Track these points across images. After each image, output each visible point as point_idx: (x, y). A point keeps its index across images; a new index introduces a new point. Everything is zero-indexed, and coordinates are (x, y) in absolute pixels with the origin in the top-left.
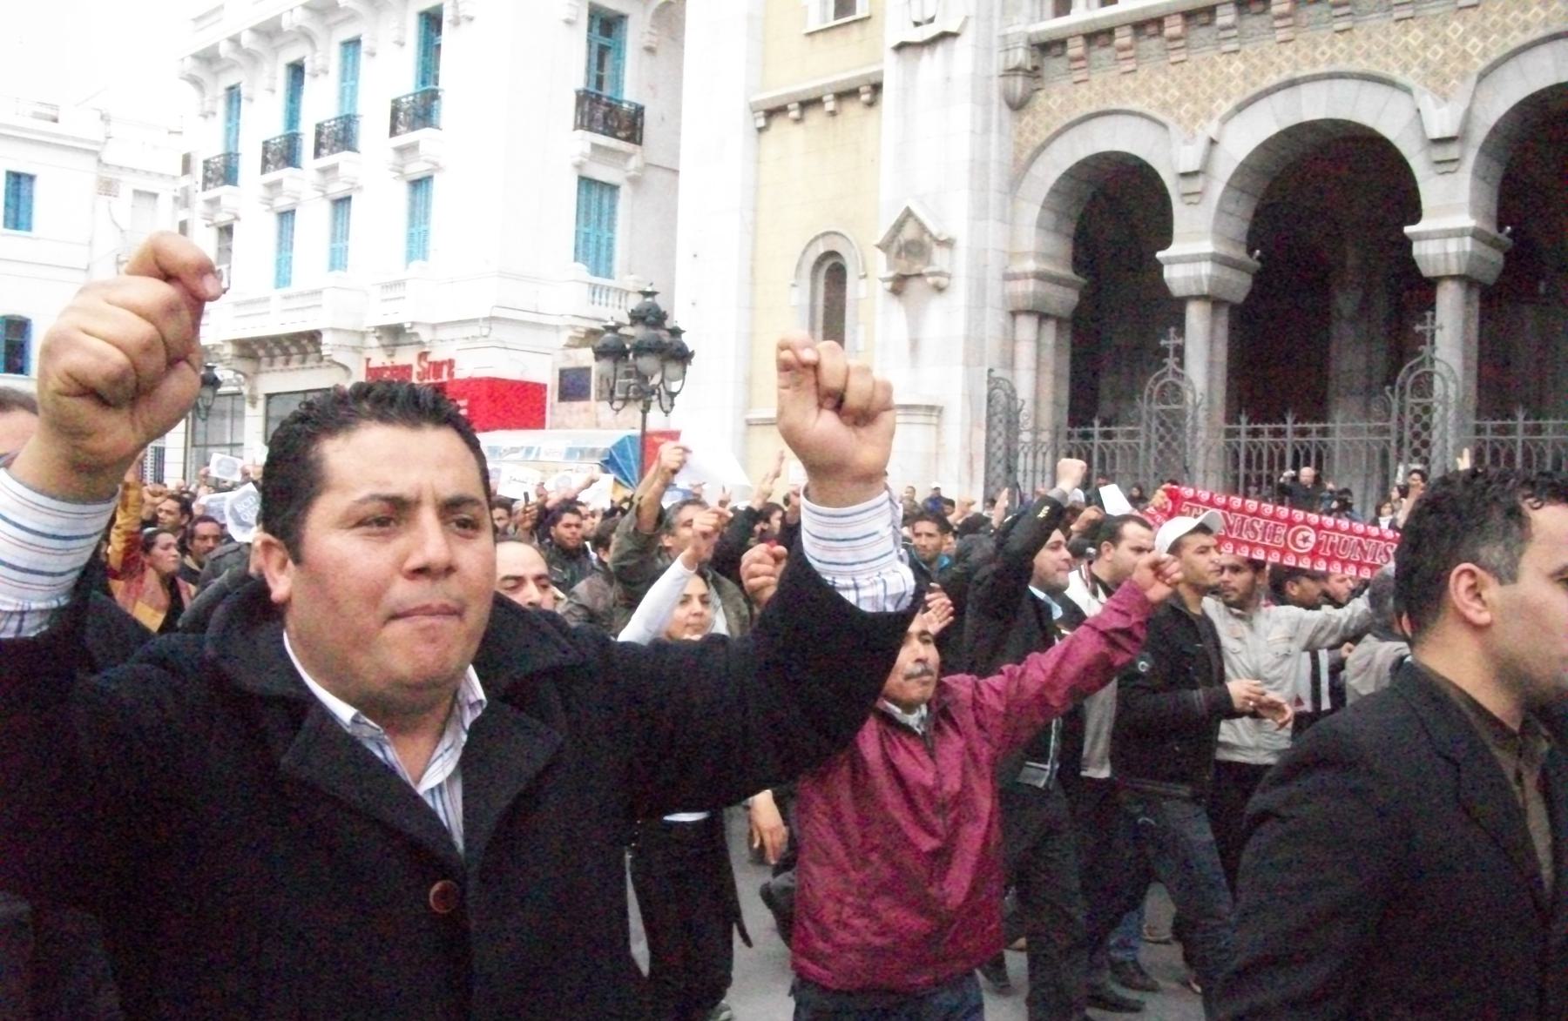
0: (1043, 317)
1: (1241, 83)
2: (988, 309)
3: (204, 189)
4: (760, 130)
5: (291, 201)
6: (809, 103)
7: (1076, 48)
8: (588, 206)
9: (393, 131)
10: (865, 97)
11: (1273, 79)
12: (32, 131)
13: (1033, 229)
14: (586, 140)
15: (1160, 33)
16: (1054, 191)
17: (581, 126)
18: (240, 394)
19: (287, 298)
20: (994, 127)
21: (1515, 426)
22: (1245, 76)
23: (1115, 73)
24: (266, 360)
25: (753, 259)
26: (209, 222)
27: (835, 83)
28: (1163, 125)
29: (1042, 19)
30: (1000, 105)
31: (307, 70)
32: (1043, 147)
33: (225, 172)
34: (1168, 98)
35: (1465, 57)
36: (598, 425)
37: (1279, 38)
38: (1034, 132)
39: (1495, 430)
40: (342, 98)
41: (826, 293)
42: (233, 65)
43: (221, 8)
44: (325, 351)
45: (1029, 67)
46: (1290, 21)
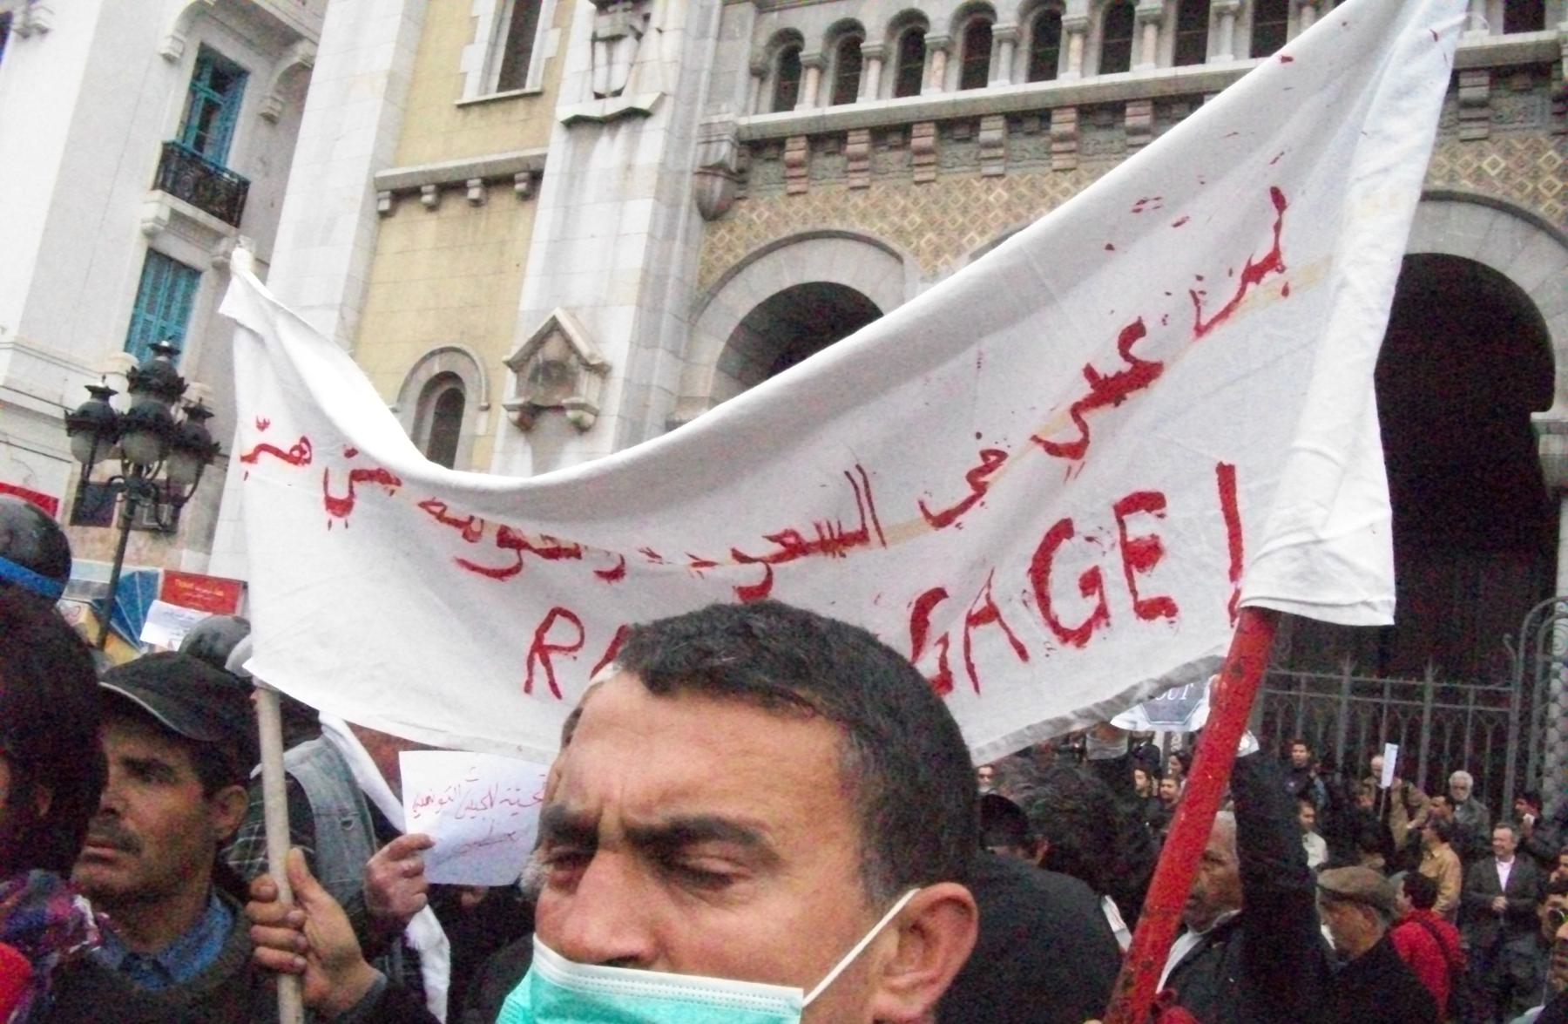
1: (1000, 213)
4: (384, 215)
6: (450, 187)
7: (796, 151)
10: (520, 187)
13: (713, 369)
15: (905, 145)
16: (745, 324)
20: (680, 233)
21: (1423, 687)
22: (1008, 207)
23: (843, 187)
27: (487, 165)
28: (899, 258)
29: (756, 112)
30: (690, 211)
32: (738, 269)
34: (905, 223)
37: (1056, 164)
39: (1395, 691)
41: (434, 429)
45: (733, 168)
46: (1073, 145)
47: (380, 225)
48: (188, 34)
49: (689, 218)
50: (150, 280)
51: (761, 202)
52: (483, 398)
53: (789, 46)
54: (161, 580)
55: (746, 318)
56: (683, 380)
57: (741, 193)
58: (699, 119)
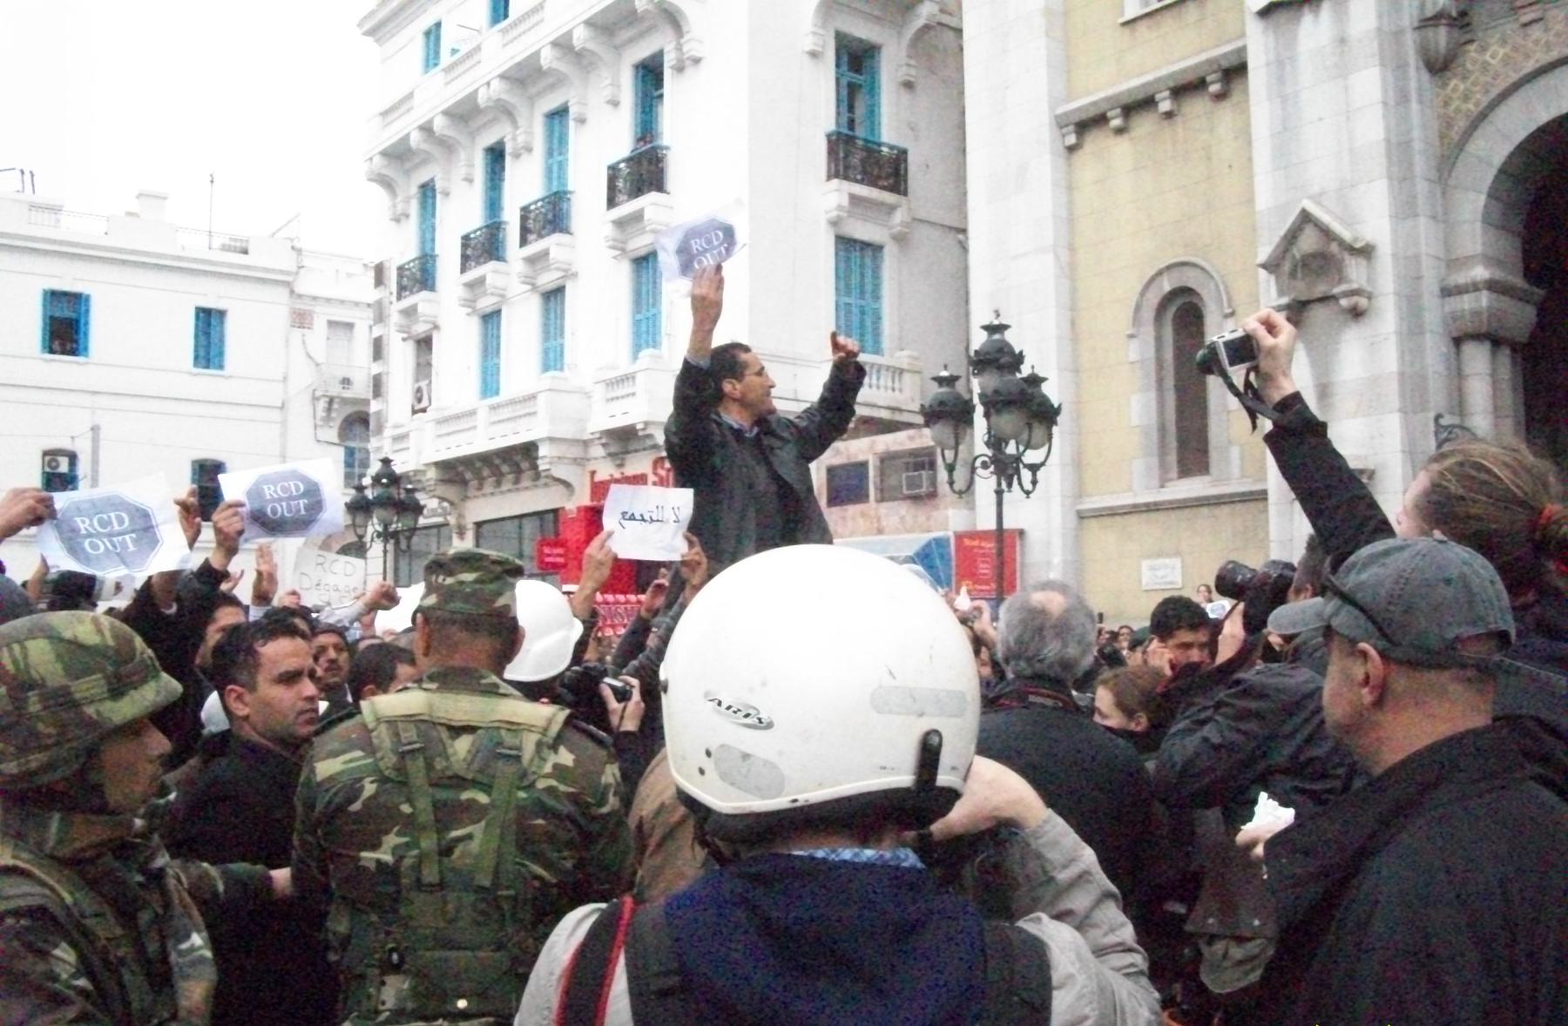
0: (1496, 342)
2: (1428, 336)
3: (399, 298)
4: (1071, 149)
5: (494, 300)
6: (1137, 106)
8: (848, 267)
9: (612, 202)
12: (222, 264)
13: (1478, 225)
14: (837, 194)
16: (1502, 171)
17: (837, 176)
18: (446, 525)
19: (493, 408)
20: (1414, 96)
24: (474, 483)
25: (1073, 308)
26: (405, 335)
27: (1171, 76)
30: (1418, 69)
31: (509, 149)
32: (1483, 116)
33: (421, 276)
36: (880, 531)
38: (1466, 98)
40: (549, 179)
41: (1176, 341)
42: (426, 160)
43: (410, 96)
44: (542, 465)
47: (1068, 159)
48: (824, 26)
49: (1419, 80)
50: (842, 265)
51: (1492, 41)
52: (1225, 304)
54: (952, 542)
55: (1505, 163)
56: (1447, 244)
57: (1468, 37)
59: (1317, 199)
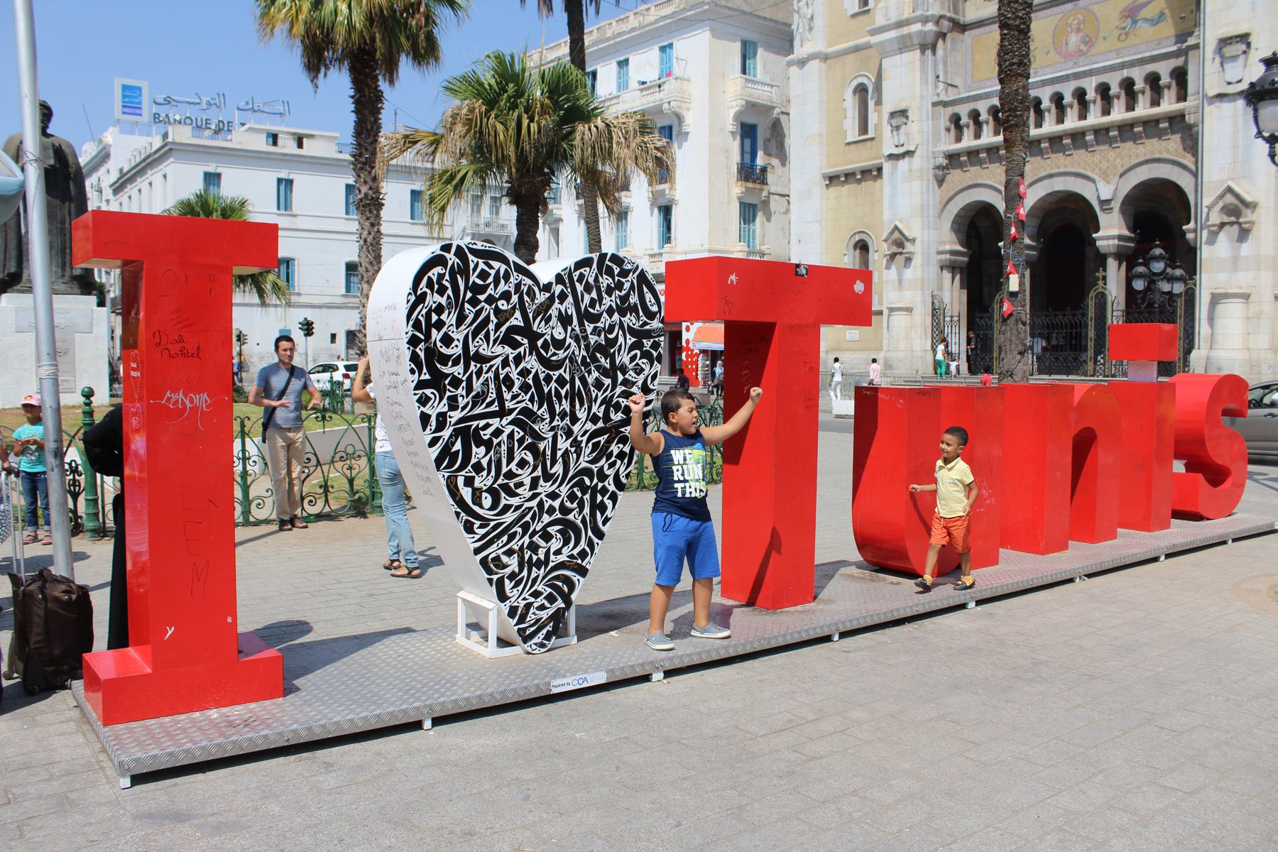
6: (849, 176)
10: (875, 173)
11: (1043, 174)
20: (931, 190)
35: (1115, 167)
53: (956, 119)
58: (930, 150)
59: (901, 220)
